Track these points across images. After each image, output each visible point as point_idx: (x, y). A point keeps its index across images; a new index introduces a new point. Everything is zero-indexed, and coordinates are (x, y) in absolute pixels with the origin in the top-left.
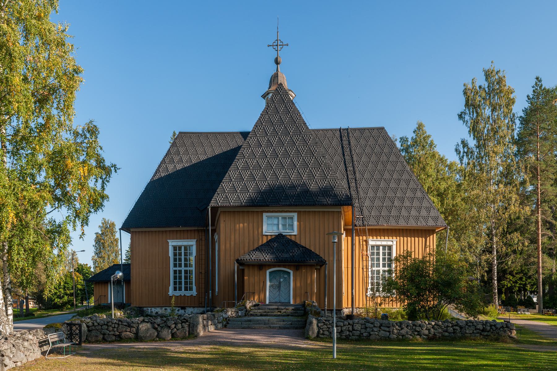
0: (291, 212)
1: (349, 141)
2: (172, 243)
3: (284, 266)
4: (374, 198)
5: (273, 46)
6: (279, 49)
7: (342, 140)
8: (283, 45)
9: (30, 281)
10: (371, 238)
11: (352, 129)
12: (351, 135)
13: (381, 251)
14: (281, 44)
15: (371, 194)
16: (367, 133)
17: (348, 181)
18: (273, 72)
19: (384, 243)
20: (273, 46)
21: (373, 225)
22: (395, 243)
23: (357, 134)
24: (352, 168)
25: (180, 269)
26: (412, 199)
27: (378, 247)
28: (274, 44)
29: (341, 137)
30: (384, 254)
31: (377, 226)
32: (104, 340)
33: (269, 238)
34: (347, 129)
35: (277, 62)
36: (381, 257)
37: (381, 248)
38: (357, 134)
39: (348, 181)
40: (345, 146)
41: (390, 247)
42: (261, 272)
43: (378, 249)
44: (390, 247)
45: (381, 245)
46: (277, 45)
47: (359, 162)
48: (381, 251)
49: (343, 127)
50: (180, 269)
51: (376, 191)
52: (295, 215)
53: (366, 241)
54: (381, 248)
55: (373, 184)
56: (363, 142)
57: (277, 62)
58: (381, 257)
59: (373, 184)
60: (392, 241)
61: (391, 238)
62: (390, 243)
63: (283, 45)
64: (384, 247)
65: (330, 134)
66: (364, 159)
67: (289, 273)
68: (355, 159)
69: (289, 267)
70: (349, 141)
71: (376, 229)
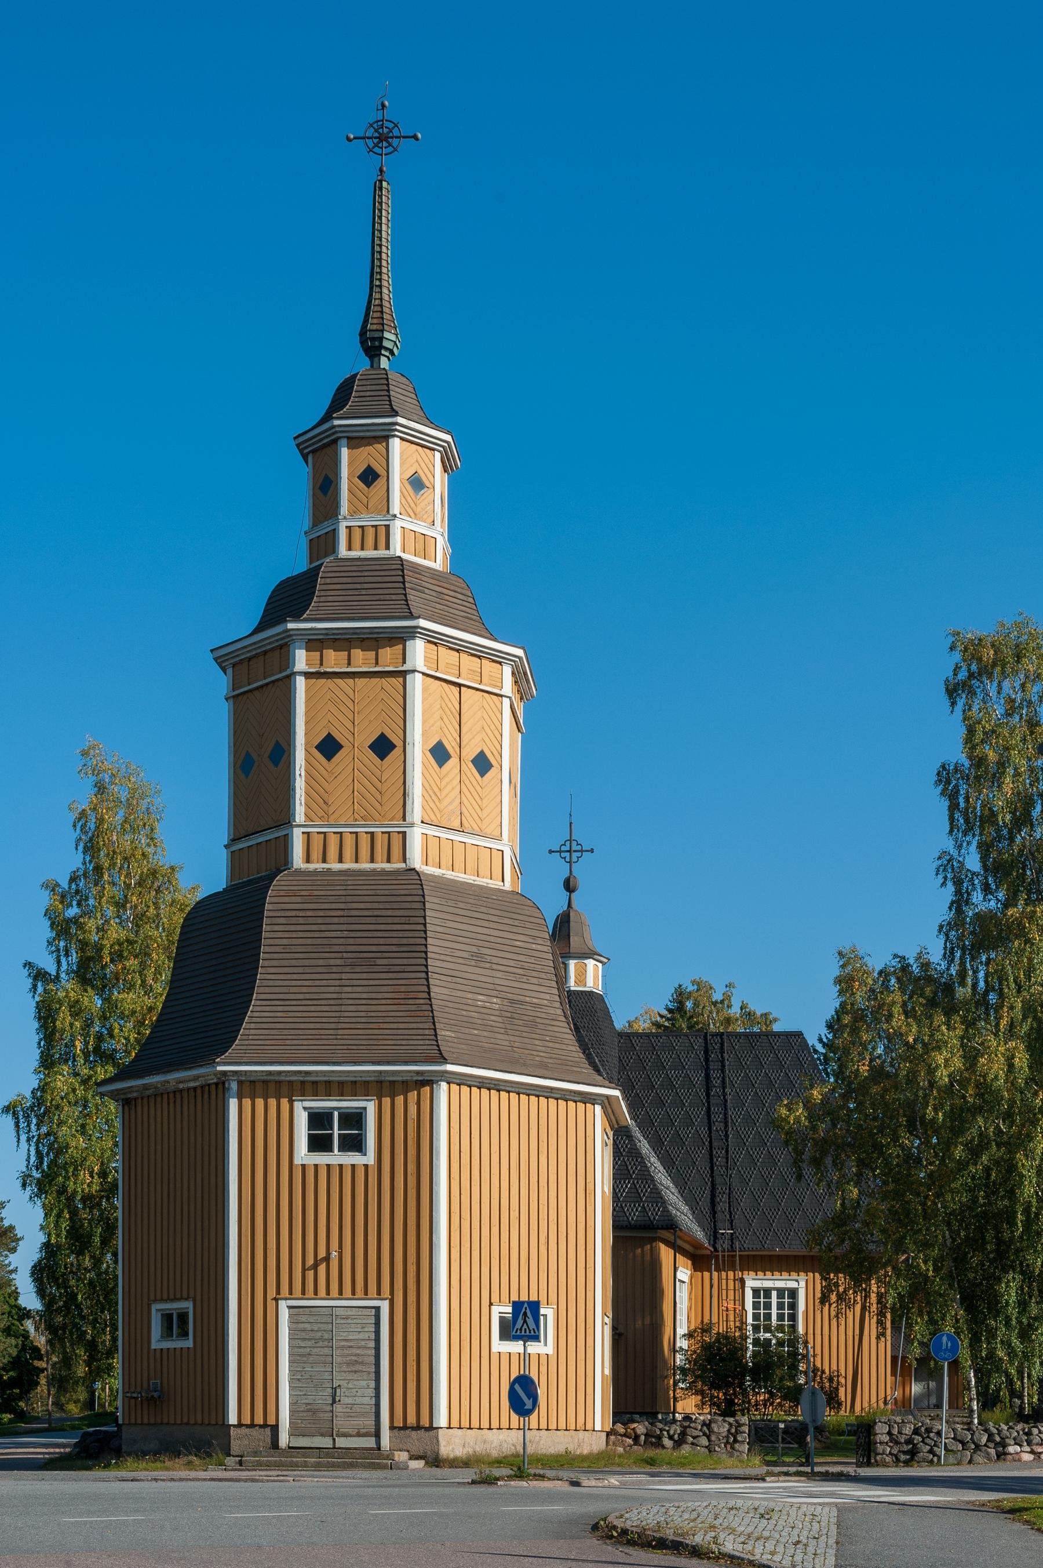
2: (752, 1282)
5: (560, 852)
6: (574, 859)
7: (707, 1060)
8: (582, 851)
9: (69, 1312)
10: (746, 1273)
14: (579, 848)
17: (711, 1154)
20: (560, 852)
21: (753, 1250)
22: (803, 1284)
27: (767, 1292)
28: (563, 848)
29: (706, 1052)
30: (780, 1306)
31: (761, 1250)
32: (91, 1522)
35: (569, 886)
36: (774, 1311)
37: (774, 1294)
39: (711, 1154)
41: (793, 1293)
44: (793, 1293)
45: (774, 1289)
53: (742, 1282)
54: (774, 1294)
57: (569, 886)
58: (774, 1311)
60: (797, 1281)
61: (794, 1275)
62: (792, 1285)
63: (582, 851)
64: (781, 1292)
71: (761, 1256)
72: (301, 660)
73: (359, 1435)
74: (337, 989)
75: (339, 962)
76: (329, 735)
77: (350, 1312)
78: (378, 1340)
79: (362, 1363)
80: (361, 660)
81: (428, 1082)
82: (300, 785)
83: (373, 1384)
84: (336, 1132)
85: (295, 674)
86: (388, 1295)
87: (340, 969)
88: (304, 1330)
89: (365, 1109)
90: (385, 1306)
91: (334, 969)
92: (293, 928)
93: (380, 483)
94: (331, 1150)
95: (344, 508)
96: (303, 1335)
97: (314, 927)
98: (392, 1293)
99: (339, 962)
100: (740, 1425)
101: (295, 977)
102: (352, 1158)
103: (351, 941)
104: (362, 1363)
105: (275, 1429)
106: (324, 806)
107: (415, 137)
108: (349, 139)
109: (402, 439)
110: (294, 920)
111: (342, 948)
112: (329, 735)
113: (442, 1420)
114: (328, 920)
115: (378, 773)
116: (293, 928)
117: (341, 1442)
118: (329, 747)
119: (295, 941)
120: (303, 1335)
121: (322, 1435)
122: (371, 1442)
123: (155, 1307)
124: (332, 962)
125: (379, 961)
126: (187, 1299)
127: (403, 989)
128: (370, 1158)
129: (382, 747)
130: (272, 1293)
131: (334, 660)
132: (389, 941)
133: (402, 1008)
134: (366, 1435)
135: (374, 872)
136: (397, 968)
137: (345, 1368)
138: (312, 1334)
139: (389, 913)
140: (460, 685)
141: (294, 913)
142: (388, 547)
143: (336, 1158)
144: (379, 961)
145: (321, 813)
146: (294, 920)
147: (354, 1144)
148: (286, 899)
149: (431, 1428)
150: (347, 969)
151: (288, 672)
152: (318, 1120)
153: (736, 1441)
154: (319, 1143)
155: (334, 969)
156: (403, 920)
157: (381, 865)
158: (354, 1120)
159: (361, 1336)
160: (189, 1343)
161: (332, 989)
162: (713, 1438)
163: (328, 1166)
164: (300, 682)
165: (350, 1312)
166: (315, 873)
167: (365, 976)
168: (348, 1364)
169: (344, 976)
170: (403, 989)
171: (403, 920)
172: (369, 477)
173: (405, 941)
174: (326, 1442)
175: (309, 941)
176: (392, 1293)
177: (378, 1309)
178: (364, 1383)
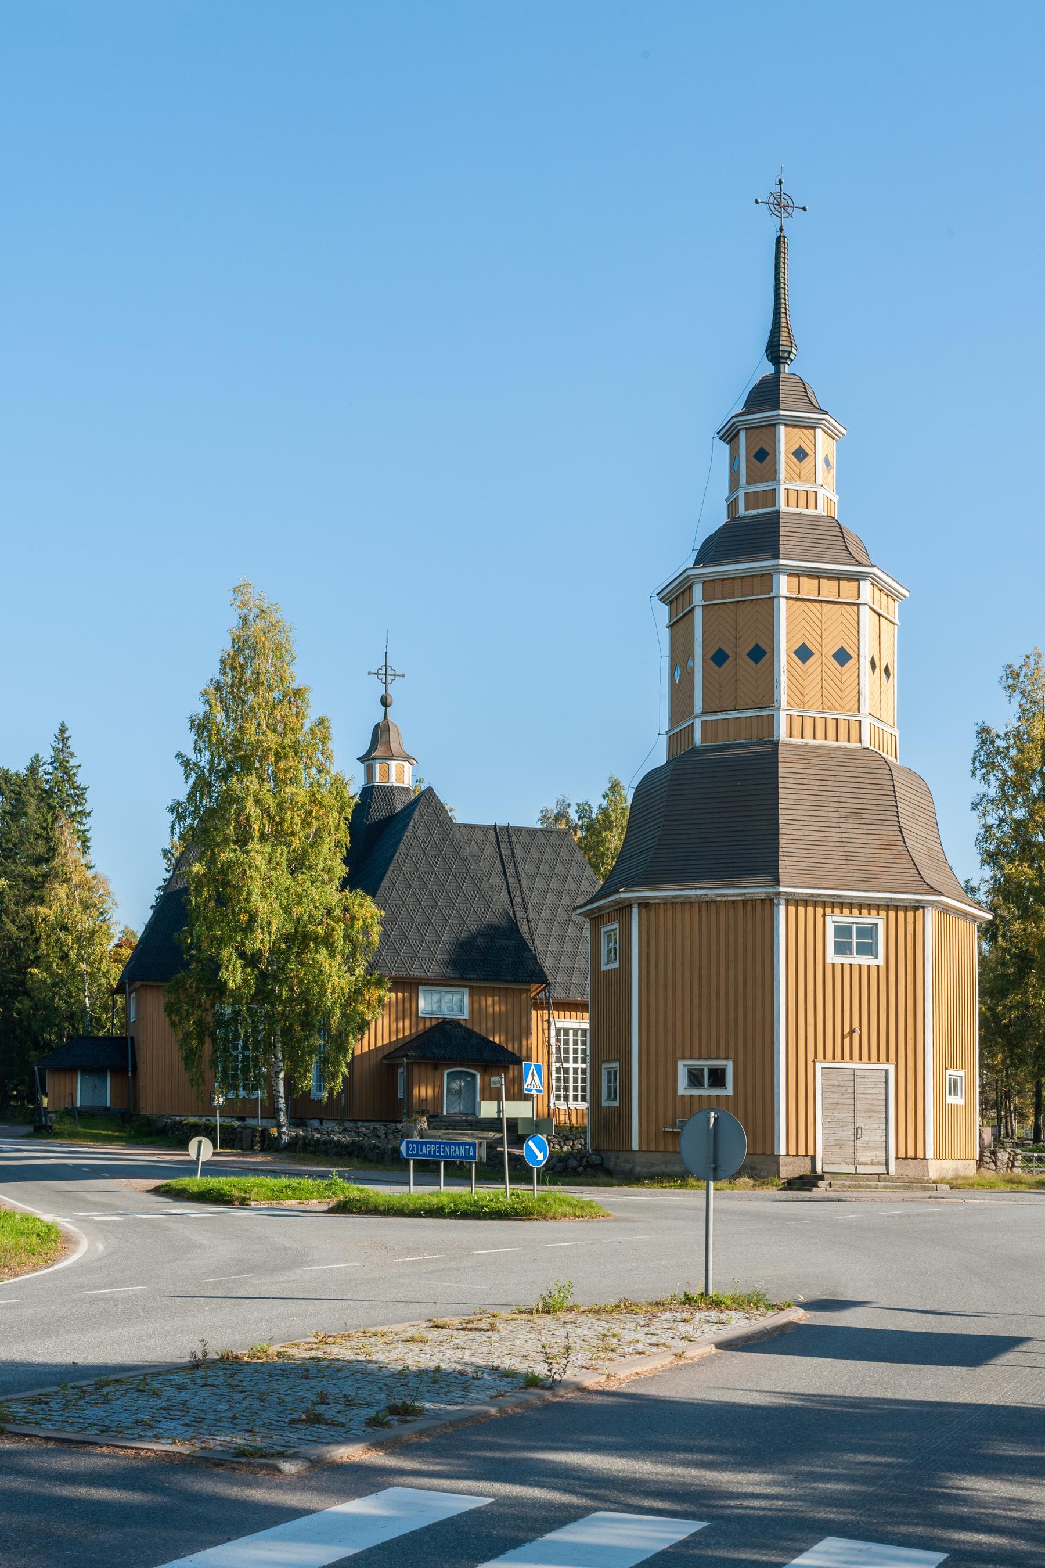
0: (459, 986)
1: (512, 849)
3: (469, 1067)
4: (560, 953)
11: (514, 828)
12: (514, 839)
13: (571, 1038)
15: (554, 946)
16: (540, 839)
18: (380, 719)
19: (576, 1026)
23: (524, 838)
24: (520, 900)
25: (576, 1066)
26: (547, 879)
27: (566, 1031)
33: (434, 1023)
34: (508, 828)
35: (385, 702)
37: (571, 1032)
38: (524, 838)
40: (506, 860)
42: (437, 1073)
43: (566, 1034)
46: (386, 673)
47: (531, 889)
48: (571, 1038)
49: (502, 823)
50: (576, 1066)
51: (562, 940)
52: (466, 991)
54: (571, 1032)
55: (556, 930)
56: (535, 854)
59: (556, 930)
64: (576, 1031)
65: (479, 835)
66: (539, 884)
67: (474, 1076)
68: (524, 884)
69: (475, 1067)
70: (512, 849)
72: (784, 585)
73: (872, 1164)
74: (839, 835)
75: (836, 814)
76: (757, 646)
77: (867, 1073)
78: (887, 1094)
79: (875, 1111)
80: (829, 589)
81: (918, 907)
82: (783, 679)
83: (883, 1126)
84: (855, 940)
85: (779, 597)
86: (894, 1061)
87: (837, 820)
88: (833, 1086)
89: (876, 925)
90: (892, 1069)
91: (833, 820)
92: (800, 787)
93: (808, 460)
94: (851, 954)
95: (782, 475)
96: (833, 1089)
97: (815, 788)
98: (736, 1053)
99: (836, 814)
100: (1016, 1155)
101: (806, 823)
102: (865, 961)
103: (843, 800)
104: (875, 1111)
105: (814, 1158)
106: (801, 697)
107: (804, 209)
108: (757, 202)
109: (823, 430)
110: (800, 781)
111: (837, 805)
112: (757, 646)
113: (930, 1154)
114: (824, 783)
115: (839, 676)
116: (800, 787)
117: (861, 1169)
118: (804, 653)
119: (802, 797)
120: (833, 1089)
121: (847, 1164)
122: (882, 1169)
123: (681, 1064)
124: (831, 814)
125: (864, 816)
126: (727, 1058)
127: (885, 837)
128: (880, 961)
129: (842, 657)
130: (811, 1057)
131: (809, 587)
132: (870, 802)
133: (888, 852)
134: (878, 1163)
135: (838, 749)
136: (878, 822)
137: (863, 1114)
138: (839, 1089)
139: (868, 781)
140: (879, 615)
141: (799, 776)
142: (816, 508)
143: (855, 960)
144: (864, 816)
145: (798, 702)
146: (800, 781)
147: (867, 949)
148: (792, 765)
149: (925, 1159)
150: (843, 820)
151: (772, 595)
152: (842, 931)
153: (1013, 1166)
154: (842, 948)
155: (833, 820)
156: (878, 787)
157: (843, 743)
158: (868, 932)
159: (874, 1091)
160: (683, 1087)
161: (834, 834)
162: (999, 1164)
163: (869, 966)
164: (783, 601)
165: (867, 1073)
166: (796, 745)
167: (855, 826)
168: (865, 1111)
169: (841, 825)
170: (885, 837)
171: (878, 787)
172: (800, 454)
173: (881, 803)
174: (851, 1169)
175: (813, 798)
176: (736, 1053)
177: (886, 1071)
178: (876, 1126)
